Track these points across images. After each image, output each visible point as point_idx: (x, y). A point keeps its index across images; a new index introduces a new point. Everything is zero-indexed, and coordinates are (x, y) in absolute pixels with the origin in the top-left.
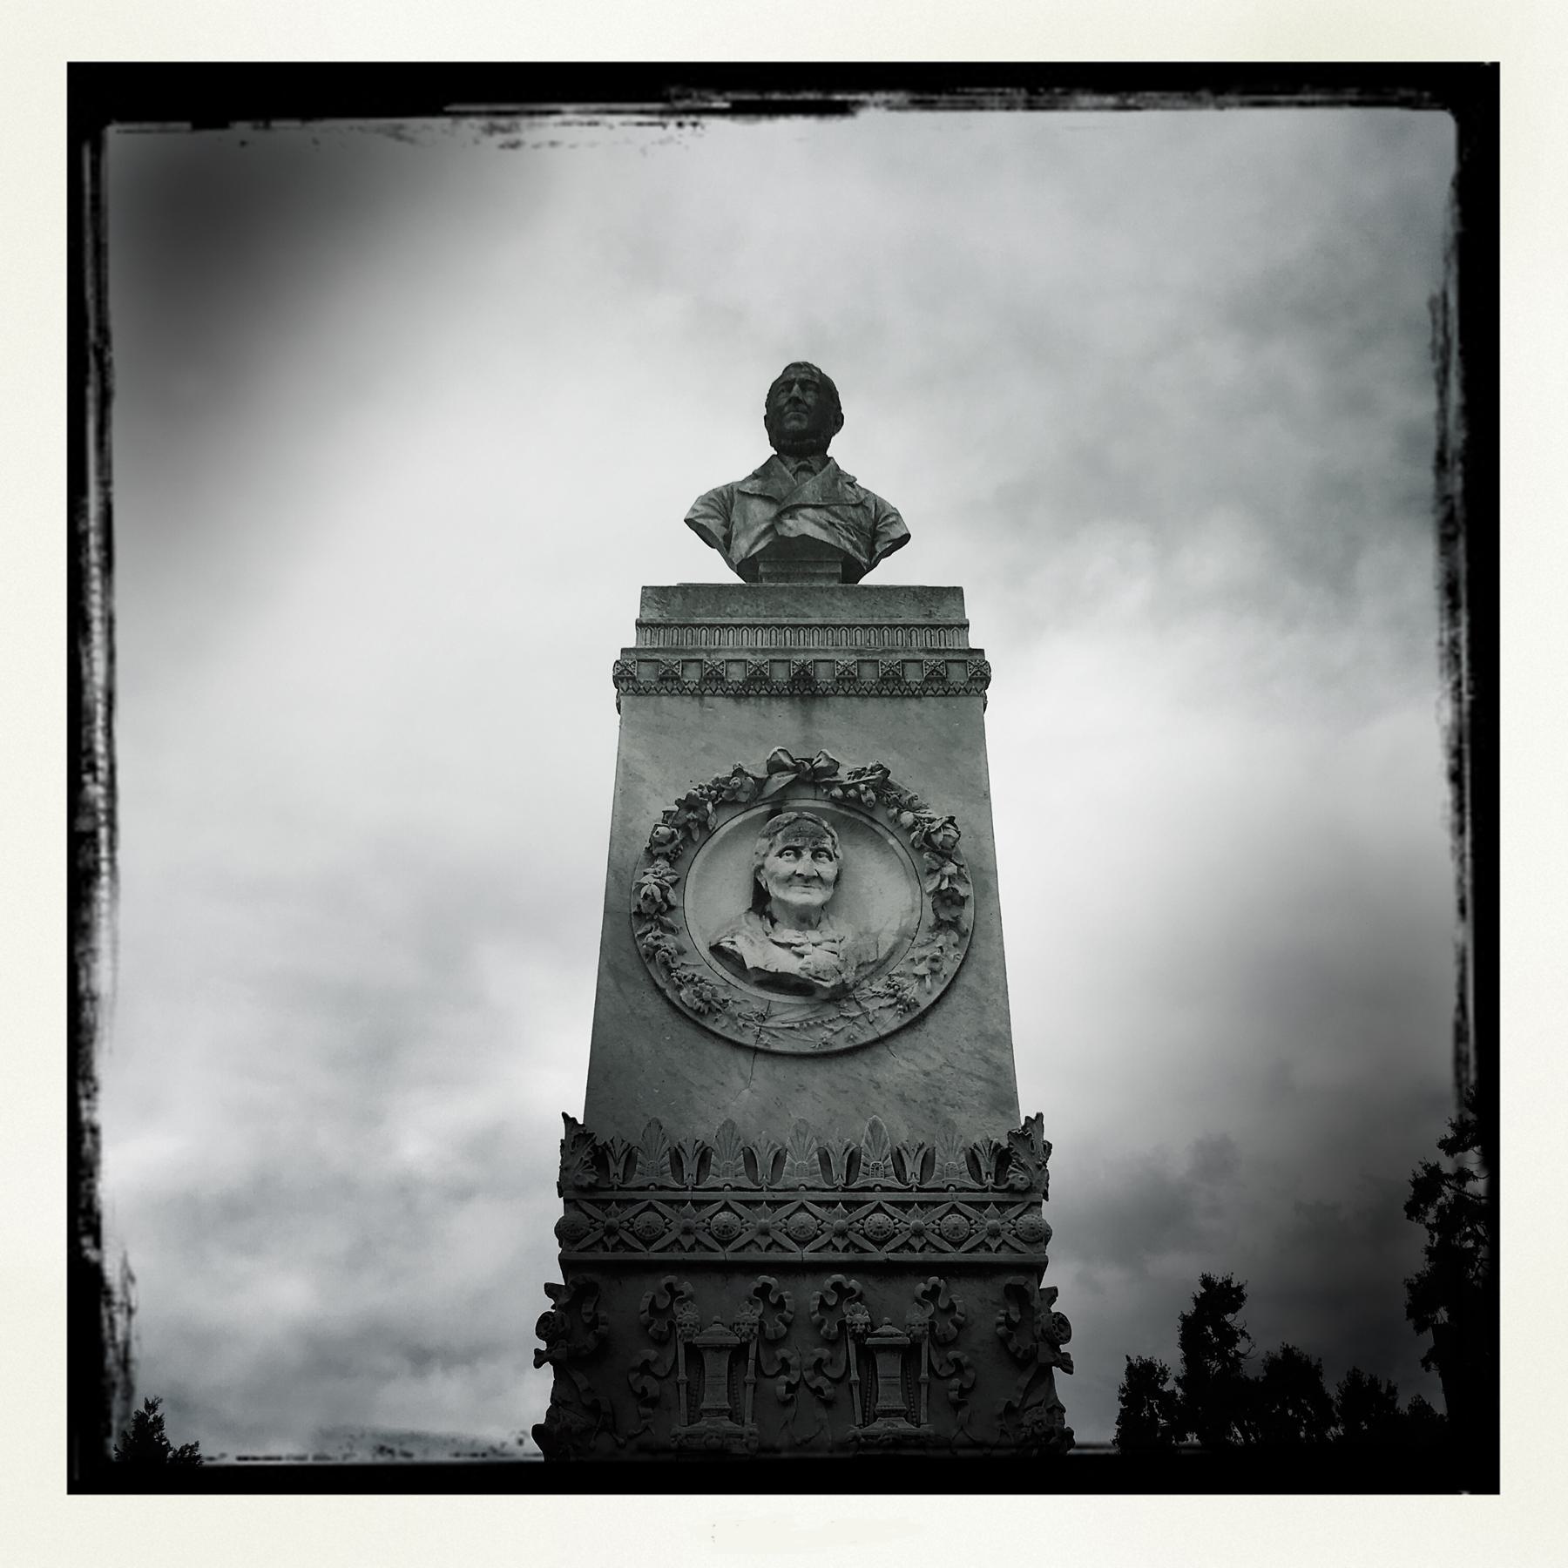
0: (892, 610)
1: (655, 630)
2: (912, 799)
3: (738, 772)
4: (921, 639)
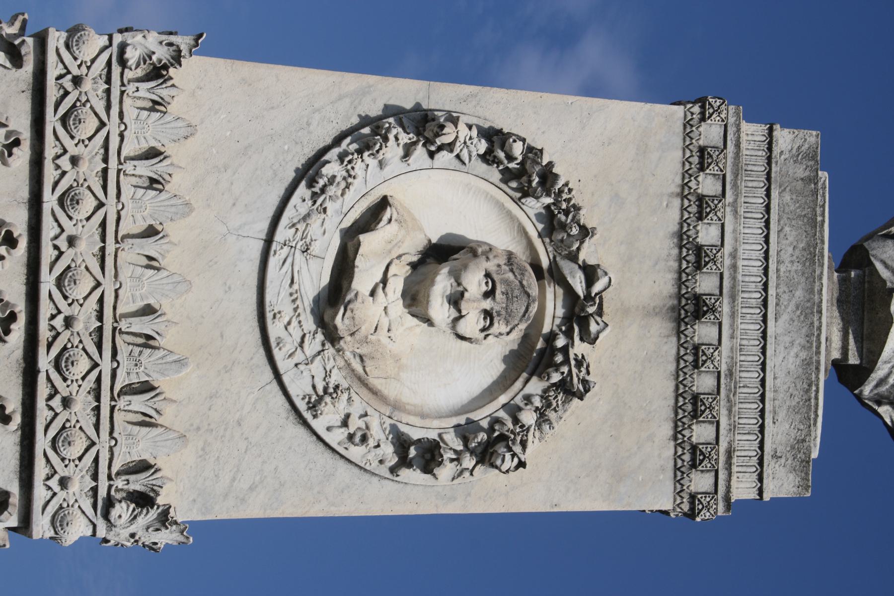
0: (782, 415)
1: (765, 146)
2: (550, 423)
3: (585, 232)
4: (746, 445)
